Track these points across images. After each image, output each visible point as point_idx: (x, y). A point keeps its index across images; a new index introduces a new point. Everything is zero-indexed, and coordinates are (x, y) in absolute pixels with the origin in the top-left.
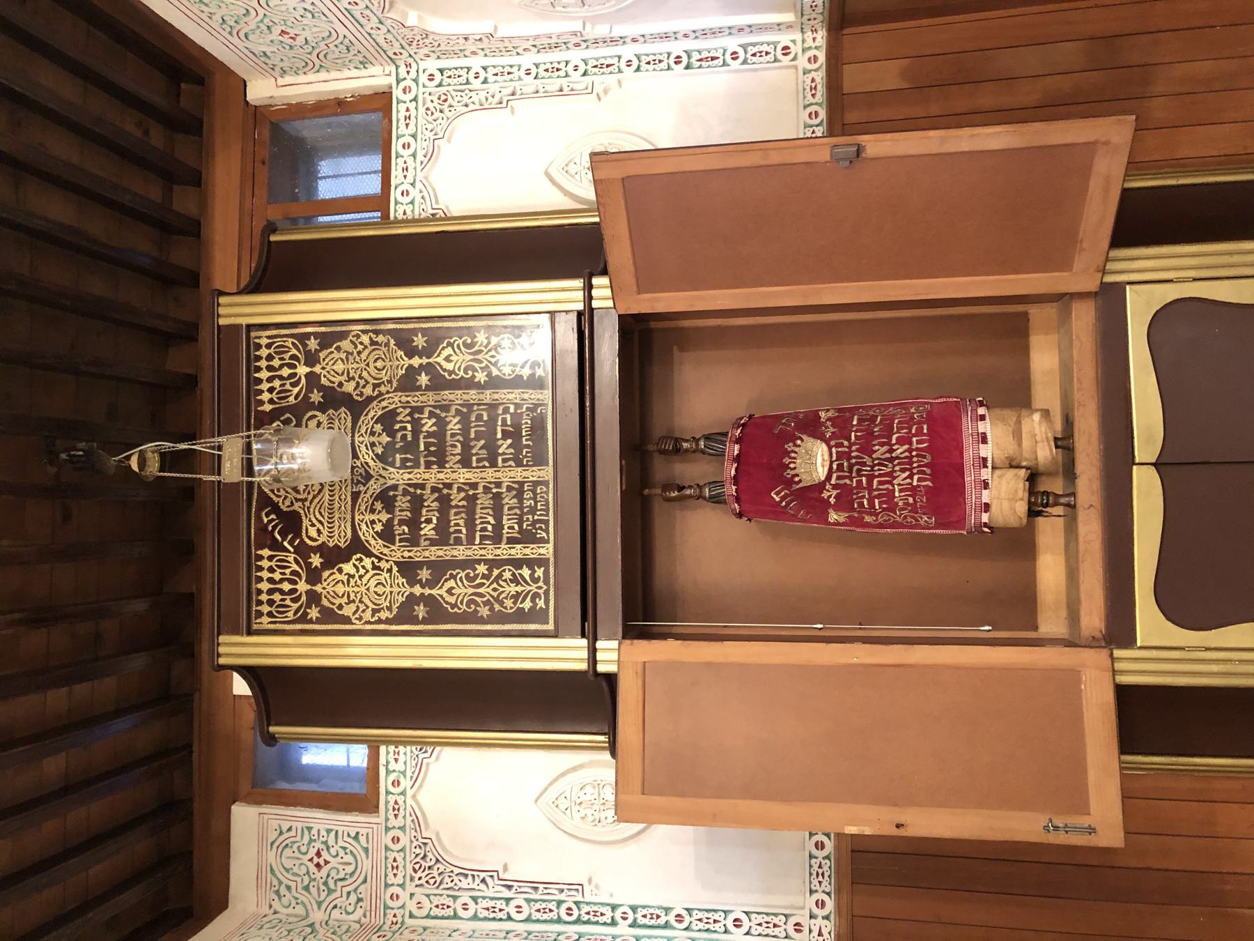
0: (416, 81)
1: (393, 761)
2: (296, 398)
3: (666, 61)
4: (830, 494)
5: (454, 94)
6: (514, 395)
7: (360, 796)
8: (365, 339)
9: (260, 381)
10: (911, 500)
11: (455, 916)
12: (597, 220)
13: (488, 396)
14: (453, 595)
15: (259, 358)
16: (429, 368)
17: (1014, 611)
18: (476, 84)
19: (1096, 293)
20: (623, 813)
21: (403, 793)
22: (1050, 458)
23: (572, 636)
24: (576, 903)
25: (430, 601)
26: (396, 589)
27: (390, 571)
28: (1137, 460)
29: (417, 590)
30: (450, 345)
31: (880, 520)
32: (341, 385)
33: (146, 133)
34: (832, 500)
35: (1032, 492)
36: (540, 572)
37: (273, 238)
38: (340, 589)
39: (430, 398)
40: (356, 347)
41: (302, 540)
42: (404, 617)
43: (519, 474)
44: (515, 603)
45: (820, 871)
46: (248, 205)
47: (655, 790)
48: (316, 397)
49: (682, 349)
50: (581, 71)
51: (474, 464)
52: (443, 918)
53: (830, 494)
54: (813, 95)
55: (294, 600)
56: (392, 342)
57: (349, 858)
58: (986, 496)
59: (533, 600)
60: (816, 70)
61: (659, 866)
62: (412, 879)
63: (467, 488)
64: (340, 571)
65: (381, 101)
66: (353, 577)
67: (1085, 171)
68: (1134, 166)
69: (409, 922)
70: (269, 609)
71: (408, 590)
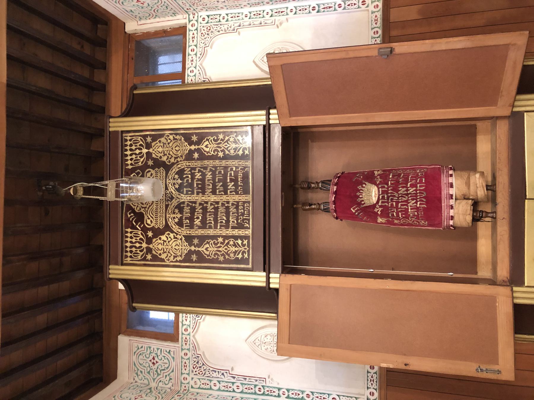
0: (197, 21)
1: (185, 321)
2: (142, 163)
3: (308, 9)
4: (378, 210)
5: (214, 26)
6: (236, 163)
7: (170, 334)
8: (171, 137)
9: (127, 155)
10: (416, 213)
11: (211, 389)
12: (270, 83)
13: (224, 163)
14: (208, 251)
15: (126, 145)
16: (198, 150)
17: (464, 266)
18: (223, 22)
19: (509, 116)
20: (280, 351)
21: (189, 334)
22: (483, 195)
23: (260, 271)
24: (263, 386)
25: (198, 253)
26: (184, 248)
27: (181, 239)
28: (528, 197)
29: (193, 248)
30: (208, 140)
31: (402, 222)
32: (161, 157)
33: (82, 47)
34: (379, 213)
35: (475, 210)
36: (245, 242)
37: (135, 92)
38: (160, 247)
39: (199, 164)
40: (167, 141)
41: (144, 225)
42: (191, 259)
43: (237, 198)
44: (234, 255)
45: (372, 379)
46: (126, 77)
47: (297, 340)
48: (150, 163)
49: (312, 141)
50: (270, 15)
51: (218, 193)
52: (205, 389)
53: (378, 210)
54: (376, 23)
55: (141, 251)
56: (183, 139)
57: (166, 361)
58: (452, 213)
59: (242, 254)
60: (377, 12)
61: (297, 373)
62: (192, 371)
63: (214, 203)
64: (160, 239)
65: (182, 30)
66: (166, 241)
67: (504, 58)
68: (528, 54)
69: (191, 390)
70: (131, 254)
71: (189, 248)
